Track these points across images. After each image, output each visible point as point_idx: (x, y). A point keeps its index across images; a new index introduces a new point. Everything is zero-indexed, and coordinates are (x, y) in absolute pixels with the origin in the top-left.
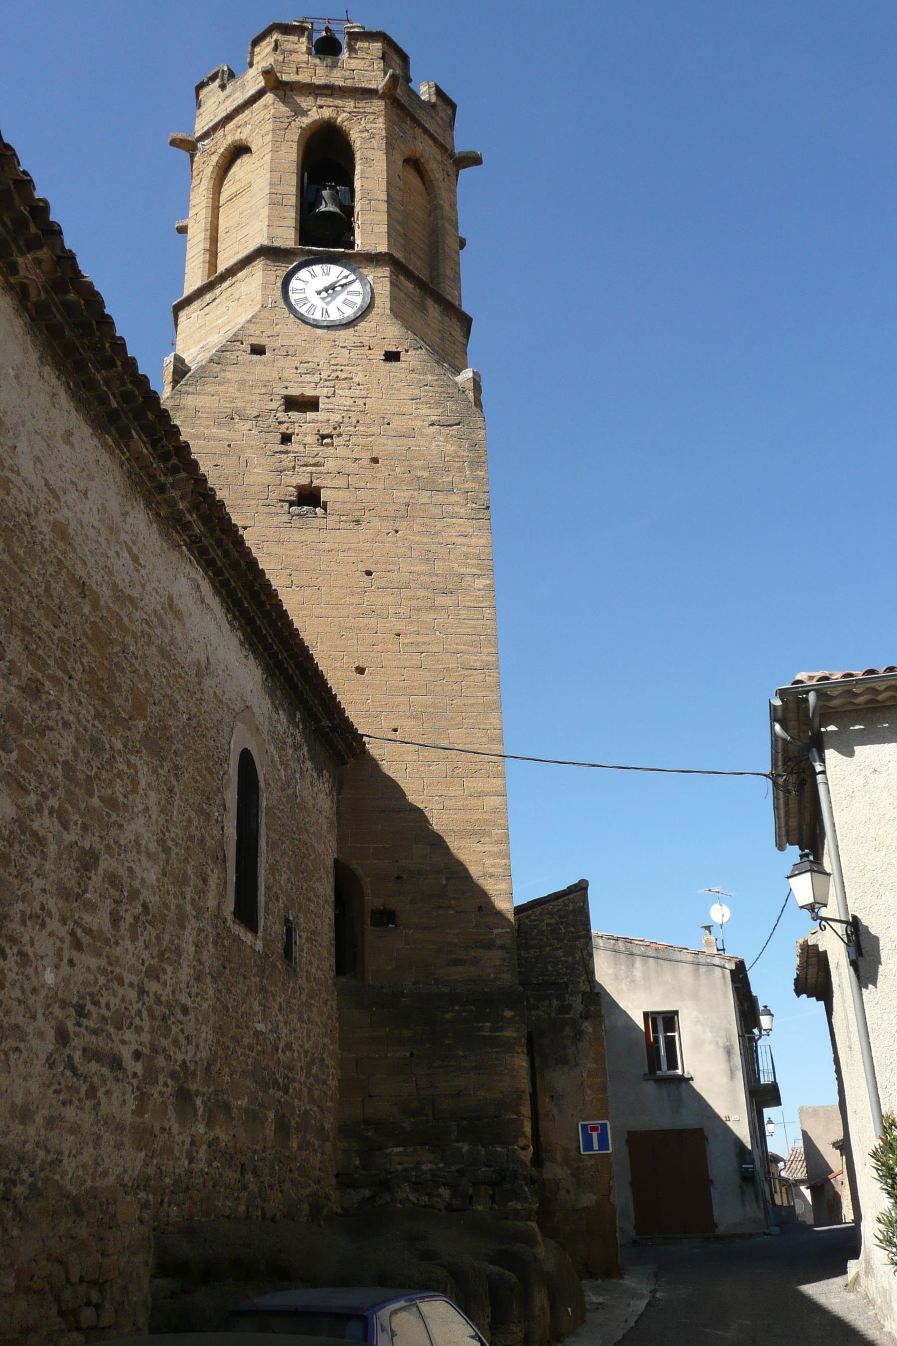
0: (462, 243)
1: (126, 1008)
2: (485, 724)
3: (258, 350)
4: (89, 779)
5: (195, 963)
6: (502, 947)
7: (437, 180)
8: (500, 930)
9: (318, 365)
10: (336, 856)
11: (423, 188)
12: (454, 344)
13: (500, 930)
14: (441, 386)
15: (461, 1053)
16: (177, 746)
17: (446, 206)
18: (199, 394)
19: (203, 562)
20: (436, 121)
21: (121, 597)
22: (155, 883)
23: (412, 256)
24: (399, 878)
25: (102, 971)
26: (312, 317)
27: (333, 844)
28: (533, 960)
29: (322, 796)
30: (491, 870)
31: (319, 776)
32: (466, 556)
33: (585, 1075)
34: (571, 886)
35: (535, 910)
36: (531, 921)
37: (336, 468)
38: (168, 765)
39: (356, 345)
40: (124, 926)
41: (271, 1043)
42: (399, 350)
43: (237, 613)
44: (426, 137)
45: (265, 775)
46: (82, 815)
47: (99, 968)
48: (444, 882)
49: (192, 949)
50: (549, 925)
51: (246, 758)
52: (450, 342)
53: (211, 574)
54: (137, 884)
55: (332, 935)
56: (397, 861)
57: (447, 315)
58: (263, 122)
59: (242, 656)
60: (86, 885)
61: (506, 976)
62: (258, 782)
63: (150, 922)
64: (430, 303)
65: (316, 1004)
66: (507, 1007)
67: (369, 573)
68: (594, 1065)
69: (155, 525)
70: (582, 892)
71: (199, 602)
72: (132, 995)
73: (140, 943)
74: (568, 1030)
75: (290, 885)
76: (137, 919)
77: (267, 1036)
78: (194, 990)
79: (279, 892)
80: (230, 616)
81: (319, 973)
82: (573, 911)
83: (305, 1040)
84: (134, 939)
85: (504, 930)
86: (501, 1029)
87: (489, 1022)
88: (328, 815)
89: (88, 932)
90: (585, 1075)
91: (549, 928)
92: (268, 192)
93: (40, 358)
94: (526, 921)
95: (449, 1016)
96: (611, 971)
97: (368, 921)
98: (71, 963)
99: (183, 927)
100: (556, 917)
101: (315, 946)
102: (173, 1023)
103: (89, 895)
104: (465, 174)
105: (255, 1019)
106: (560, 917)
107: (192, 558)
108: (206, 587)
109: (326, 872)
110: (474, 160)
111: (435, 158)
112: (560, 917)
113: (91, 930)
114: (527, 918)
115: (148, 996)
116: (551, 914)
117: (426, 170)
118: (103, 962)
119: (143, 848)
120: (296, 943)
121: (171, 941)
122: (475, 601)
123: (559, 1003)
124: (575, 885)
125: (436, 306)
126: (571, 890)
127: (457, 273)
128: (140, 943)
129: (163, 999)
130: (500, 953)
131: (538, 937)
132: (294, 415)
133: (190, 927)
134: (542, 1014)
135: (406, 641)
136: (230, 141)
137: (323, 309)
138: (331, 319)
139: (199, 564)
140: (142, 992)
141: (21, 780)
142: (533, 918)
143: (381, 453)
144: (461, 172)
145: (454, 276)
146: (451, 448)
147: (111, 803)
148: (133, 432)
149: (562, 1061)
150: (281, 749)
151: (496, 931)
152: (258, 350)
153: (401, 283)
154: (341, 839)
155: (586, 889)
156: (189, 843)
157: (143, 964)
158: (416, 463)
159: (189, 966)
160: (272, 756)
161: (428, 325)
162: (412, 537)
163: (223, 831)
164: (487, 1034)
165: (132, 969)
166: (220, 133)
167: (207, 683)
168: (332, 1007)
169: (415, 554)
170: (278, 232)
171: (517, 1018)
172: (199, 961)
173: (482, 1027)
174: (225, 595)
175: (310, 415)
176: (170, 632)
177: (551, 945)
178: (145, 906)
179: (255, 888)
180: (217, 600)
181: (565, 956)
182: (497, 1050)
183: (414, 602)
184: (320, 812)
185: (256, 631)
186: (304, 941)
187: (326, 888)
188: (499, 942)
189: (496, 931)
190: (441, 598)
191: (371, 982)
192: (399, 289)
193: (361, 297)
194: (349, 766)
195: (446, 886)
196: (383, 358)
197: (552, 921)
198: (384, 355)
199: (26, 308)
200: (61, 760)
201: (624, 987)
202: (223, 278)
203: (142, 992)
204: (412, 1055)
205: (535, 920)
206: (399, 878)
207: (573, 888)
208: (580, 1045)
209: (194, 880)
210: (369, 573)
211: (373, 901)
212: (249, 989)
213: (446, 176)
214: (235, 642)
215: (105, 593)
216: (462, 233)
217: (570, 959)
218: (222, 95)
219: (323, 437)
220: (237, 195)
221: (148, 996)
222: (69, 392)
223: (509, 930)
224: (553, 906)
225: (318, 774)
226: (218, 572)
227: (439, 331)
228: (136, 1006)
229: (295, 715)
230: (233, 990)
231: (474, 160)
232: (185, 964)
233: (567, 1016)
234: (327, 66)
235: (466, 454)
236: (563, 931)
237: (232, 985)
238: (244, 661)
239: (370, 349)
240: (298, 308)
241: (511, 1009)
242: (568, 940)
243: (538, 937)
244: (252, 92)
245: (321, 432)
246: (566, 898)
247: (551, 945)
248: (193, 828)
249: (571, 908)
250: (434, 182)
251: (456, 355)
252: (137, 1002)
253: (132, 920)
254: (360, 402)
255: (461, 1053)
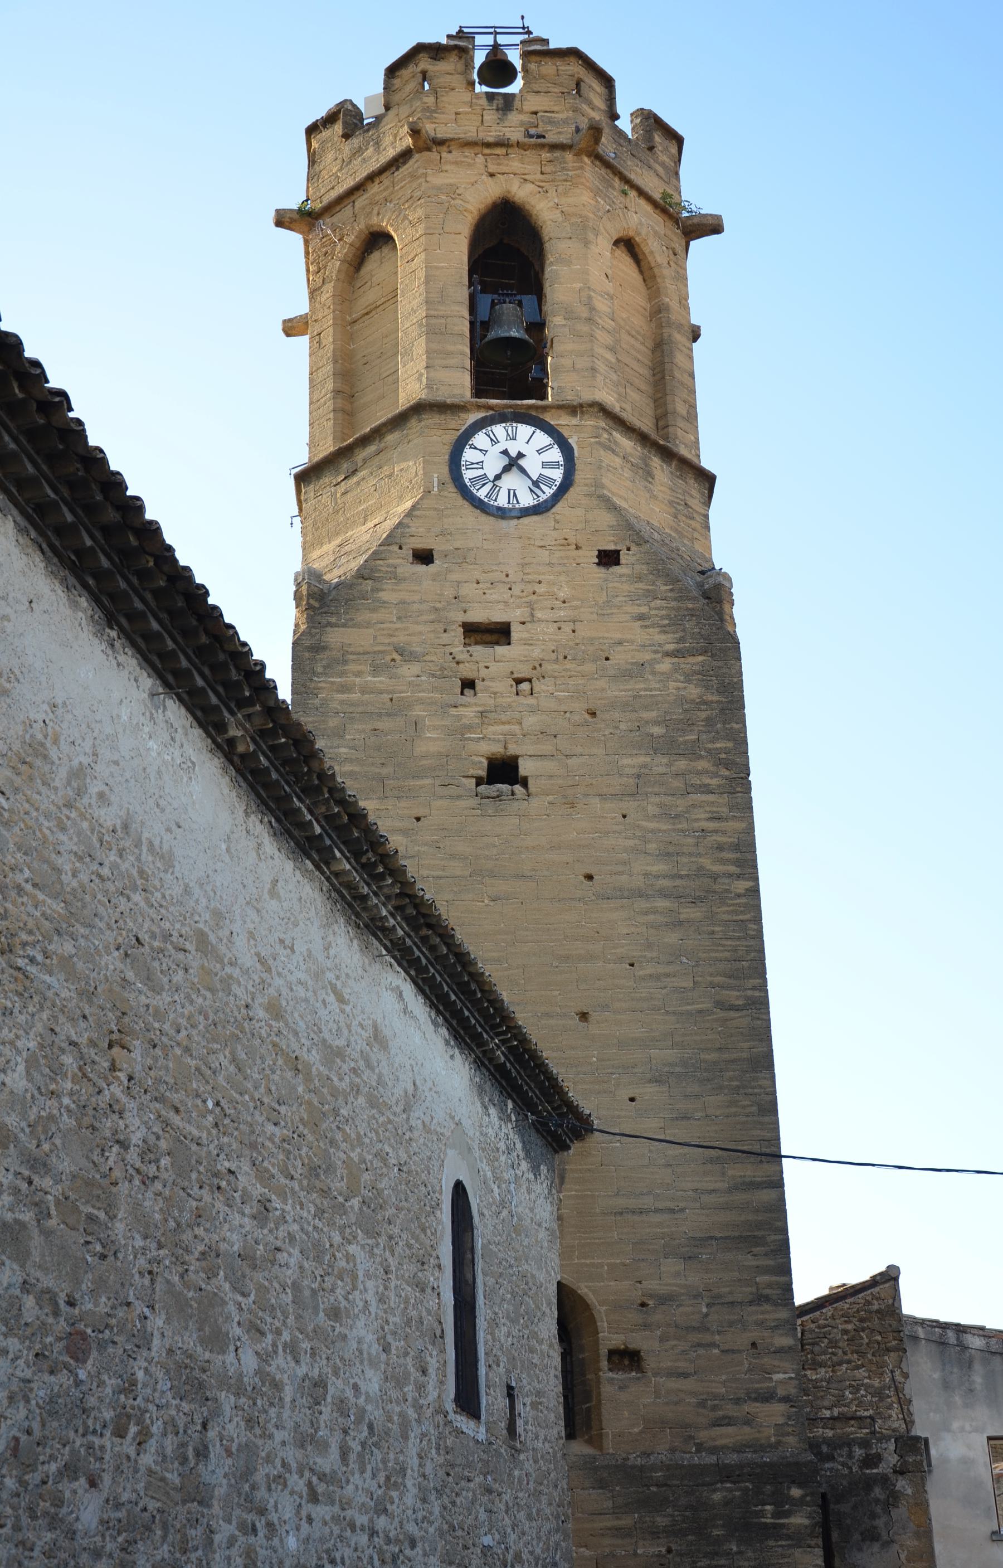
0: (695, 334)
1: (359, 1558)
2: (753, 1088)
3: (424, 557)
4: (314, 1292)
5: (420, 1479)
6: (785, 1399)
7: (659, 266)
8: (781, 1376)
9: (507, 576)
10: (559, 1278)
11: (639, 278)
12: (692, 518)
13: (781, 1376)
14: (675, 599)
15: (735, 1548)
16: (390, 1212)
17: (674, 305)
18: (344, 626)
19: (405, 964)
20: (656, 171)
21: (333, 1054)
22: (378, 1393)
23: (628, 390)
24: (643, 1305)
25: (336, 1519)
26: (496, 504)
27: (554, 1259)
28: (824, 1384)
29: (541, 1201)
30: (767, 1291)
31: (536, 1178)
32: (720, 848)
33: (903, 1557)
34: (875, 1276)
35: (824, 1311)
36: (819, 1327)
37: (538, 728)
38: (382, 1240)
39: (558, 542)
40: (352, 1457)
41: (499, 1559)
42: (618, 548)
43: (441, 1008)
44: (642, 202)
45: (478, 1205)
46: (311, 1340)
47: (333, 1518)
48: (704, 1310)
49: (416, 1461)
50: (845, 1332)
51: (459, 1190)
52: (686, 517)
53: (413, 973)
54: (361, 1401)
55: (560, 1389)
56: (640, 1282)
57: (681, 477)
58: (410, 202)
59: (447, 1058)
60: (318, 1422)
61: (791, 1440)
62: (472, 1218)
63: (375, 1445)
64: (656, 462)
65: (546, 1490)
66: (793, 1482)
67: (590, 877)
68: (916, 1543)
69: (355, 941)
70: (892, 1282)
71: (402, 1015)
72: (364, 1539)
73: (368, 1474)
74: (878, 1492)
75: (510, 1339)
76: (363, 1444)
77: (495, 1549)
78: (420, 1515)
79: (499, 1353)
80: (433, 1014)
81: (547, 1445)
82: (878, 1312)
83: (535, 1543)
84: (362, 1472)
85: (787, 1376)
86: (788, 1514)
87: (769, 1504)
88: (547, 1225)
89: (322, 1477)
90: (903, 1557)
91: (846, 1337)
92: (424, 315)
93: (246, 811)
94: (813, 1326)
95: (717, 1497)
96: (936, 1376)
97: (604, 1364)
98: (310, 1520)
99: (406, 1437)
100: (854, 1320)
101: (541, 1411)
102: (403, 1562)
103: (321, 1433)
104: (696, 245)
105: (482, 1532)
106: (862, 1320)
107: (392, 961)
108: (408, 989)
109: (549, 1304)
110: (713, 227)
111: (656, 233)
112: (862, 1320)
113: (325, 1475)
114: (813, 1322)
115: (378, 1537)
116: (847, 1317)
117: (644, 254)
118: (336, 1509)
119: (365, 1355)
120: (520, 1414)
121: (396, 1459)
122: (735, 912)
123: (862, 1451)
124: (881, 1274)
125: (665, 466)
126: (874, 1282)
127: (692, 407)
128: (368, 1474)
129: (392, 1535)
130: (781, 1408)
131: (830, 1350)
132: (479, 651)
133: (413, 1435)
134: (840, 1467)
135: (641, 973)
136: (362, 226)
137: (509, 490)
138: (522, 506)
139: (400, 965)
140: (373, 1533)
141: (259, 1322)
142: (821, 1322)
143: (599, 702)
144: (692, 243)
145: (688, 412)
146: (694, 691)
147: (335, 1314)
148: (336, 852)
149: (872, 1536)
150: (492, 1161)
151: (777, 1377)
152: (424, 557)
153: (615, 442)
154: (565, 1254)
155: (896, 1279)
156: (408, 1330)
157: (372, 1499)
158: (646, 715)
159: (414, 1485)
160: (485, 1175)
161: (654, 497)
162: (644, 823)
163: (439, 1299)
164: (769, 1521)
165: (363, 1508)
166: (347, 212)
167: (417, 1113)
168: (563, 1489)
169: (652, 847)
170: (442, 375)
171: (808, 1498)
172: (424, 1476)
173: (761, 1511)
174: (428, 991)
175: (500, 650)
176: (377, 1071)
177: (849, 1362)
178: (371, 1427)
179: (476, 1361)
180: (421, 1000)
181: (869, 1378)
182: (784, 1543)
183: (651, 917)
184: (540, 1225)
185: (463, 1022)
186: (528, 1408)
187: (548, 1327)
188: (781, 1392)
189: (777, 1377)
190: (688, 910)
191: (611, 1451)
192: (613, 451)
193: (561, 470)
194: (571, 1152)
195: (707, 1315)
196: (597, 560)
197: (850, 1327)
198: (598, 557)
199: (231, 762)
200: (289, 1282)
201: (957, 1399)
202: (364, 441)
203: (373, 1533)
204: (669, 1551)
205: (825, 1326)
206: (643, 1305)
207: (878, 1278)
208: (895, 1513)
209: (415, 1374)
210: (590, 877)
211: (610, 1338)
212: (474, 1494)
213: (672, 256)
214: (440, 1043)
215: (314, 1057)
216: (695, 320)
217: (876, 1383)
218: (347, 148)
219: (518, 681)
220: (377, 307)
221: (378, 1537)
222: (271, 830)
223: (793, 1375)
224: (851, 1304)
225: (535, 1174)
226: (421, 970)
227: (671, 503)
228: (368, 1552)
229: (506, 1106)
230: (458, 1501)
231: (713, 227)
232: (409, 1483)
233: (875, 1471)
234: (498, 110)
235: (715, 698)
236: (866, 1340)
237: (457, 1495)
238: (450, 1063)
239: (578, 548)
240: (475, 491)
241: (800, 1485)
242: (873, 1355)
243: (830, 1350)
244: (391, 153)
245: (515, 676)
246: (869, 1292)
247: (849, 1362)
248: (411, 1308)
249: (876, 1307)
250: (656, 270)
251: (696, 535)
252: (368, 1547)
253: (359, 1448)
254: (567, 628)
255: (735, 1548)
